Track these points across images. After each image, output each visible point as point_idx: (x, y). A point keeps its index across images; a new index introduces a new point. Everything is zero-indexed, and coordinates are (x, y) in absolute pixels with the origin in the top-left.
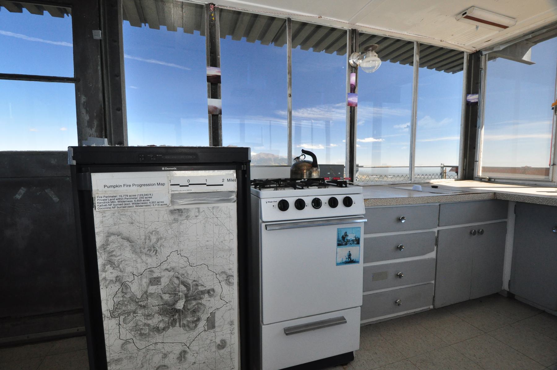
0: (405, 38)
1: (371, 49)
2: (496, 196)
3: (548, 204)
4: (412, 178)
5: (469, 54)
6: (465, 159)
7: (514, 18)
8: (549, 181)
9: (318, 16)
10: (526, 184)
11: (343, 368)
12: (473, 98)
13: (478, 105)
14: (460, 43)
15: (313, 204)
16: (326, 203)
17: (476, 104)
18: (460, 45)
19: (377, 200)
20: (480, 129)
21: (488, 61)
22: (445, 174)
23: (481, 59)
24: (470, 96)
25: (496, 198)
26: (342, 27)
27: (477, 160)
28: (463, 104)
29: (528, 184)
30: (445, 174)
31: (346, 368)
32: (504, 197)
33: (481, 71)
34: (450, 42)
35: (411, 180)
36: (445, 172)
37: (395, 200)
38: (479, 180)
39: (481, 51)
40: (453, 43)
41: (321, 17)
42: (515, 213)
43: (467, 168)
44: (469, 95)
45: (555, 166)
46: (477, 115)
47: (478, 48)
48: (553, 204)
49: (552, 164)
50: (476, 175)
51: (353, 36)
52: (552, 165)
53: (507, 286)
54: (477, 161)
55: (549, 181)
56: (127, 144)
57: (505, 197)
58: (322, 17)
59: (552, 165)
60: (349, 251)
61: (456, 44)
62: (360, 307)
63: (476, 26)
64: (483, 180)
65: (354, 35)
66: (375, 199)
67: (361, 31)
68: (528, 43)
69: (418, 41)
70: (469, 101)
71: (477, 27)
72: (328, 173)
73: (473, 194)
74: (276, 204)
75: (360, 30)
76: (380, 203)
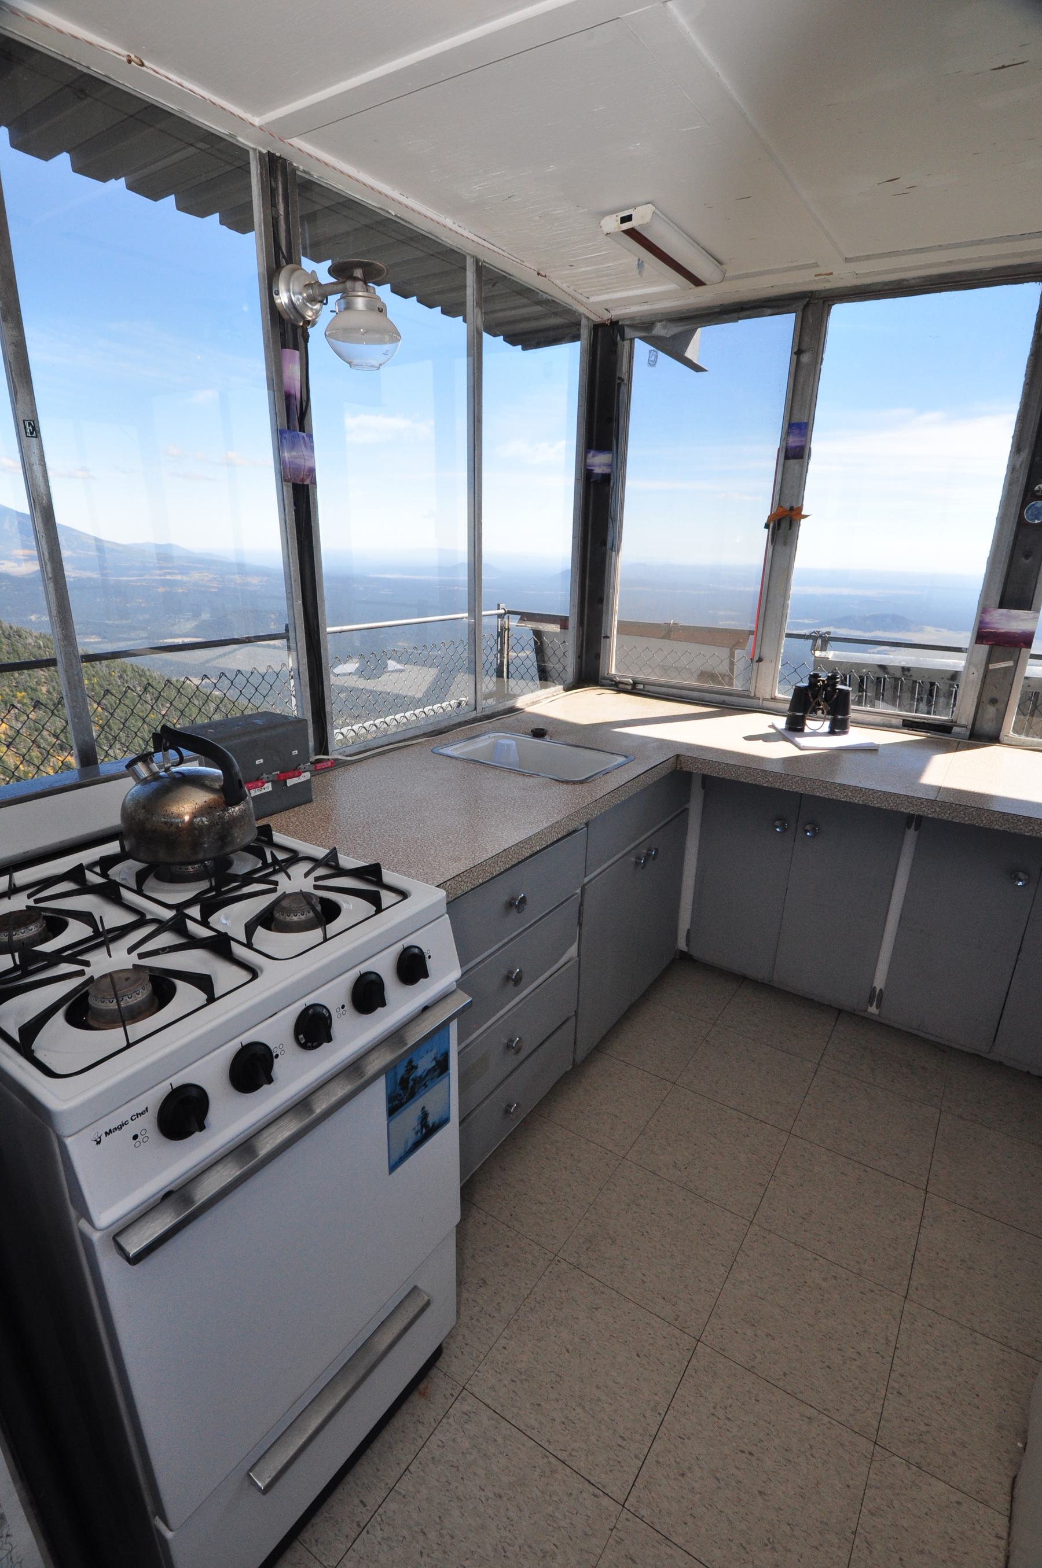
0: (442, 238)
1: (358, 273)
2: (680, 764)
3: (784, 789)
5: (594, 325)
7: (720, 263)
8: (750, 697)
9: (126, 53)
10: (705, 699)
11: (420, 1393)
13: (612, 484)
14: (580, 291)
15: (301, 1036)
16: (343, 1007)
17: (606, 478)
18: (580, 297)
19: (460, 879)
20: (614, 553)
22: (506, 632)
23: (619, 349)
24: (594, 456)
25: (681, 768)
26: (231, 135)
29: (708, 699)
30: (506, 632)
31: (426, 1388)
33: (619, 385)
34: (558, 282)
35: (475, 709)
36: (507, 627)
37: (502, 857)
38: (611, 685)
39: (620, 323)
40: (564, 286)
41: (143, 65)
42: (703, 787)
43: (584, 654)
45: (761, 663)
46: (607, 515)
47: (616, 313)
48: (794, 787)
49: (756, 658)
50: (603, 672)
51: (273, 185)
53: (685, 946)
57: (700, 766)
58: (146, 63)
60: (423, 1108)
61: (570, 290)
63: (639, 259)
64: (621, 686)
65: (276, 181)
66: (457, 878)
67: (304, 172)
69: (481, 258)
71: (640, 265)
72: (257, 762)
74: (148, 1123)
75: (301, 168)
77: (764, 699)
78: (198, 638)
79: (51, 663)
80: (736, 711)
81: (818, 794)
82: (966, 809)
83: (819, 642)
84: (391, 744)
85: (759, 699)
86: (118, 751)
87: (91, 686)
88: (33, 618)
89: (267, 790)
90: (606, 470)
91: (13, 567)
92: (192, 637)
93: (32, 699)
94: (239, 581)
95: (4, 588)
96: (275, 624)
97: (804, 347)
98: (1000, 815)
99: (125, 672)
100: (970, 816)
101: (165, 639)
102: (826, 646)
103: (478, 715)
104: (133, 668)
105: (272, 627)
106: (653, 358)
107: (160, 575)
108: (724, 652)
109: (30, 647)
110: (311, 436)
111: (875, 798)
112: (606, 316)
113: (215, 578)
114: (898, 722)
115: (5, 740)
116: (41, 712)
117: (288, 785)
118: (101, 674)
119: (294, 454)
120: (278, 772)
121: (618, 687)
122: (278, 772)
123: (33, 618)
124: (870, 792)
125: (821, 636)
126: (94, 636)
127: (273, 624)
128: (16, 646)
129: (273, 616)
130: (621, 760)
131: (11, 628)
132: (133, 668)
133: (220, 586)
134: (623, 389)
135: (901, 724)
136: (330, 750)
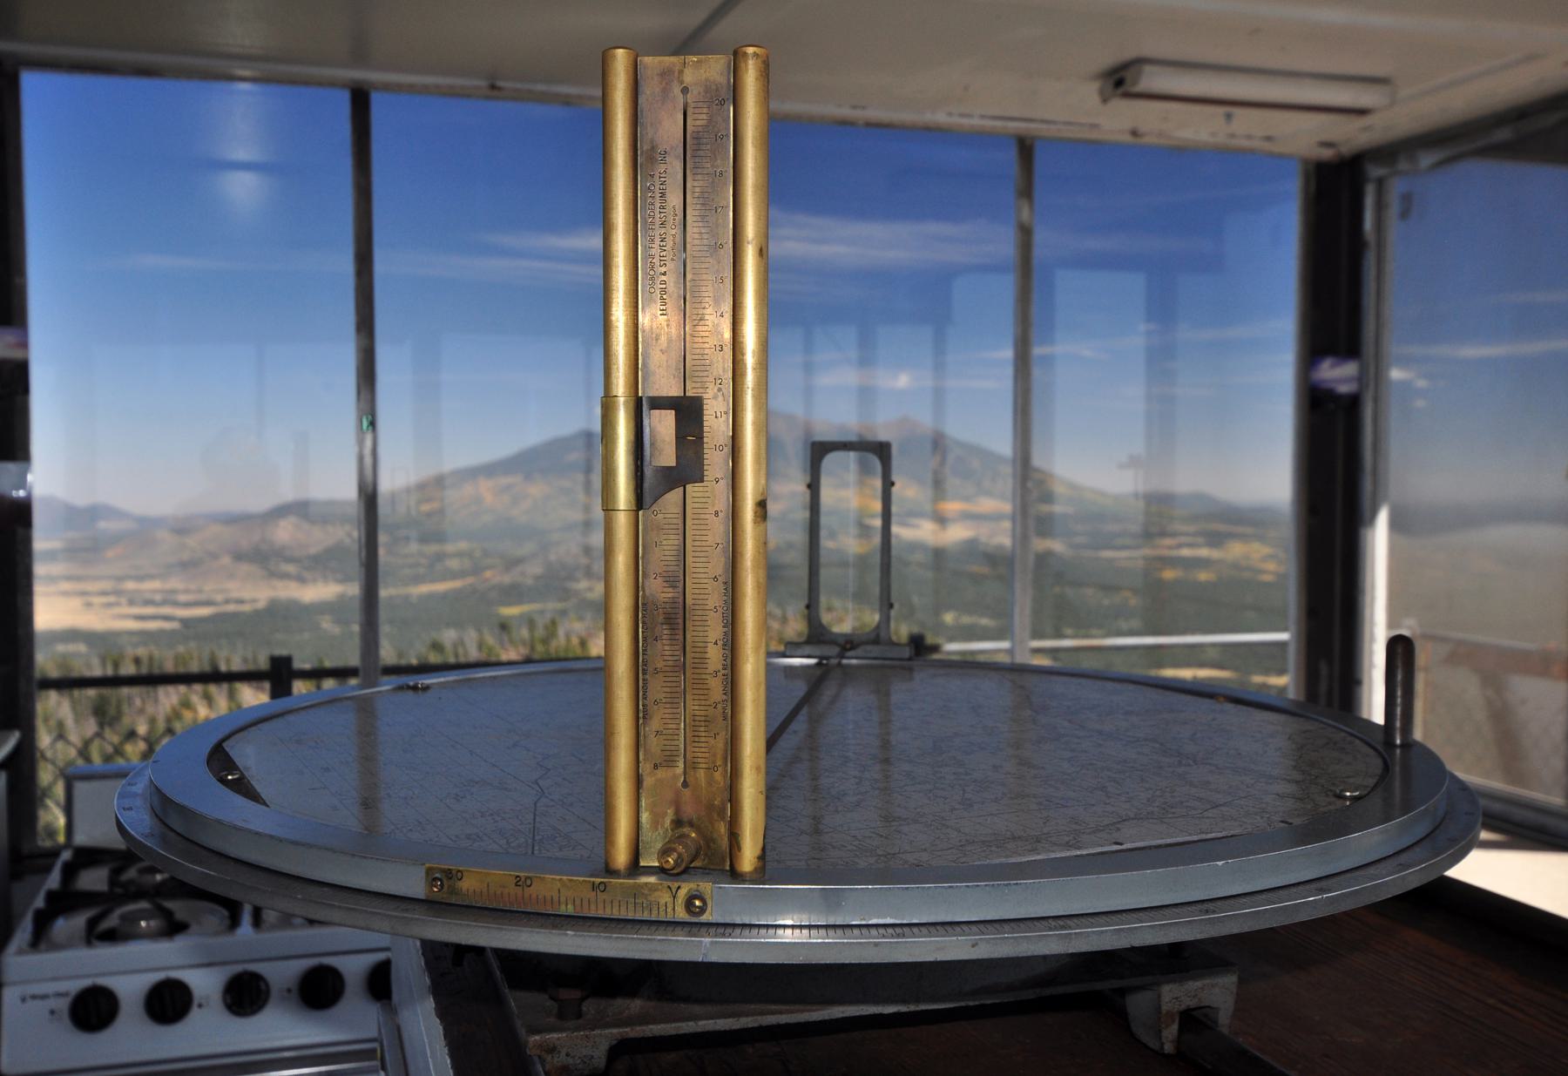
12: (1337, 374)
24: (1333, 366)
107: (1170, 548)
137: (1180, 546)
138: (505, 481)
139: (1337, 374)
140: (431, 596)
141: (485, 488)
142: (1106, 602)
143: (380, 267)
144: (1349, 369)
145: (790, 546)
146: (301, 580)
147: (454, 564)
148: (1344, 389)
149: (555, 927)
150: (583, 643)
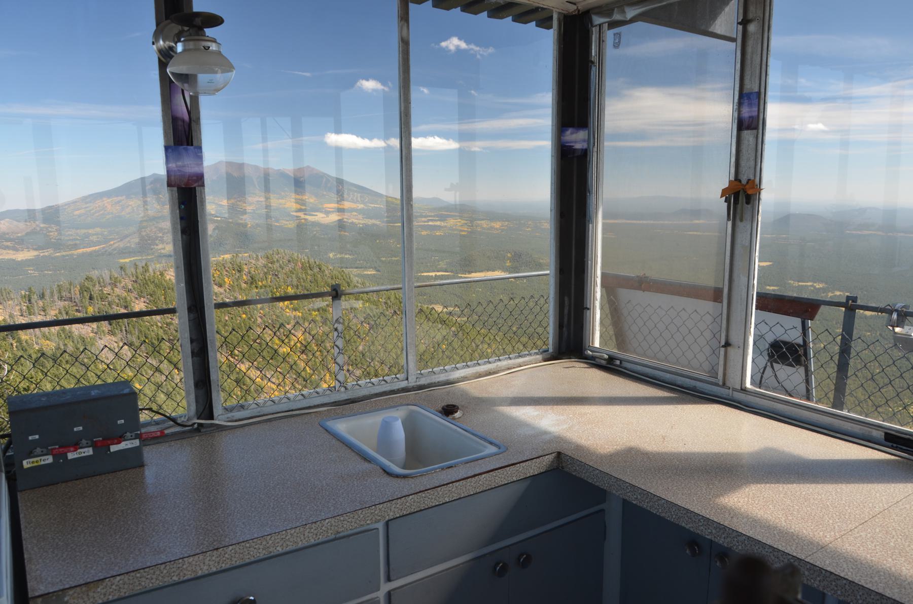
4: (409, 374)
6: (566, 299)
8: (717, 385)
12: (577, 138)
21: (609, 29)
24: (572, 133)
27: (588, 307)
28: (554, 154)
32: (576, 470)
35: (407, 379)
44: (567, 130)
45: (729, 349)
52: (723, 346)
54: (588, 309)
55: (717, 385)
56: (191, 7)
59: (723, 346)
62: (722, 287)
68: (296, 212)
70: (570, 146)
73: (491, 473)
76: (153, 581)
77: (734, 390)
78: (447, 272)
79: (172, 311)
80: (696, 399)
81: (683, 525)
82: (837, 579)
83: (895, 316)
84: (292, 410)
85: (729, 388)
86: (376, 363)
87: (364, 309)
88: (331, 255)
89: (47, 462)
90: (585, 146)
91: (323, 218)
92: (443, 272)
93: (322, 317)
94: (485, 226)
95: (315, 232)
96: (510, 262)
97: (750, 16)
98: (878, 597)
99: (389, 298)
100: (843, 590)
101: (422, 273)
102: (903, 322)
103: (410, 385)
104: (395, 296)
105: (507, 264)
106: (617, 41)
107: (425, 222)
108: (797, 322)
109: (326, 278)
110: (200, 148)
111: (740, 543)
112: (158, 53)
113: (466, 223)
114: (879, 435)
115: (300, 348)
116: (327, 328)
117: (112, 450)
118: (372, 300)
119: (179, 163)
120: (101, 439)
121: (594, 362)
122: (101, 439)
123: (331, 255)
124: (735, 534)
125: (896, 310)
126: (371, 269)
127: (508, 261)
128: (317, 277)
129: (509, 255)
130: (492, 449)
131: (315, 262)
132: (395, 296)
133: (470, 230)
134: (594, 71)
135: (883, 437)
136: (215, 414)
137: (428, 221)
138: (116, 199)
139: (577, 138)
140: (83, 254)
141: (106, 201)
142: (42, 254)
143: (414, 95)
144: (582, 135)
145: (258, 225)
146: (16, 249)
147: (94, 238)
148: (578, 146)
149: (774, 411)
150: (162, 274)
